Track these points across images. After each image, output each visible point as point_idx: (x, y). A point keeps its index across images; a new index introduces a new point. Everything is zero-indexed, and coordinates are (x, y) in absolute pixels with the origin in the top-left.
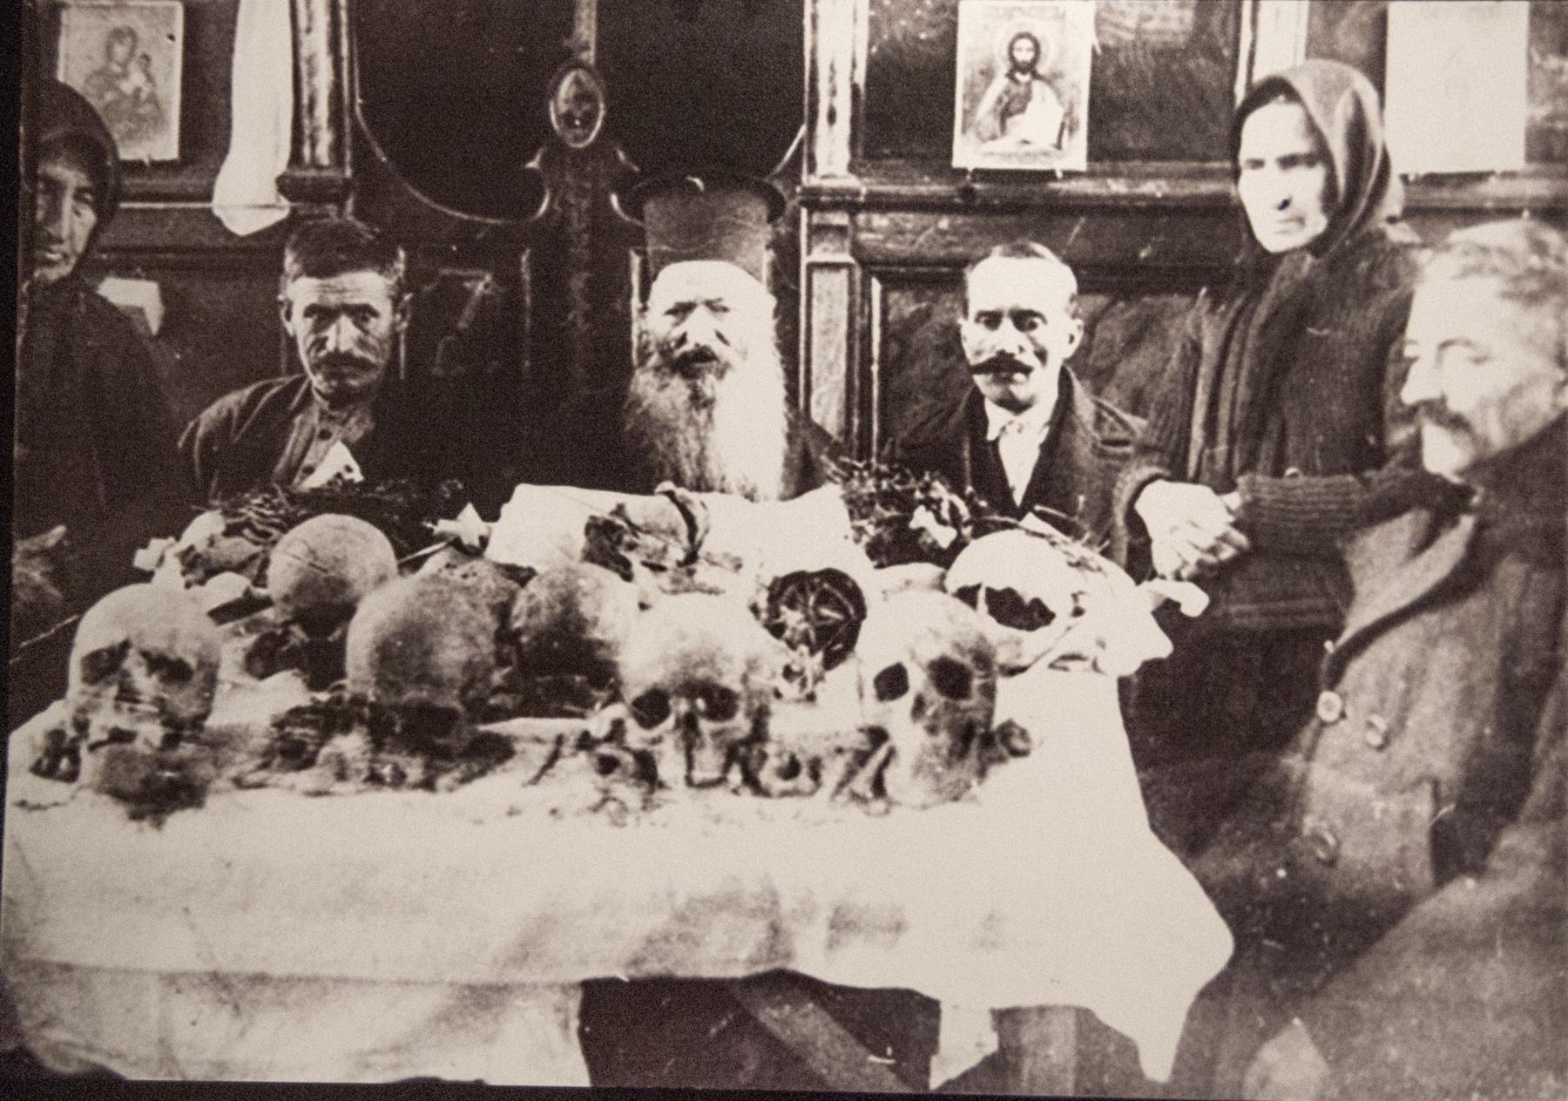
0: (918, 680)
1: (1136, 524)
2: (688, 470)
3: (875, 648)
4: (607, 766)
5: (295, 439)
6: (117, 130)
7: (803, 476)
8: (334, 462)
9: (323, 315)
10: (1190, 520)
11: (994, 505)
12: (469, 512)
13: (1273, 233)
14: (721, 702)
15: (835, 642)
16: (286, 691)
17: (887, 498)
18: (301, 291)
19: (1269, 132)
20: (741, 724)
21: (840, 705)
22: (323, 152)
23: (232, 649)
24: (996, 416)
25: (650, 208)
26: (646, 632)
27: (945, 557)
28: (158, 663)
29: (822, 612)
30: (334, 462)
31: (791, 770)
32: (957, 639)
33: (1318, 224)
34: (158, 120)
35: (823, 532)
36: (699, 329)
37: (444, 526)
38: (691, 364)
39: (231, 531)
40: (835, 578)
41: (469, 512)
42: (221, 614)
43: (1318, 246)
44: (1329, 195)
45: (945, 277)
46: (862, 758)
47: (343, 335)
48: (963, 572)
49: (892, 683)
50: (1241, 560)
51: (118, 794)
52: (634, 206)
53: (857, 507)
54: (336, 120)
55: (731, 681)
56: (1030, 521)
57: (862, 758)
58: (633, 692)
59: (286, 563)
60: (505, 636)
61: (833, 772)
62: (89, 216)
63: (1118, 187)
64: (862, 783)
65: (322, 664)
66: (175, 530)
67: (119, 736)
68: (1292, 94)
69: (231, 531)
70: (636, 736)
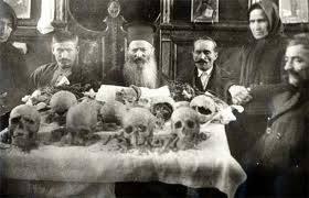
0: (183, 124)
1: (229, 94)
2: (137, 82)
3: (175, 117)
4: (121, 141)
5: (55, 75)
6: (16, 11)
7: (160, 84)
8: (64, 80)
9: (61, 50)
10: (238, 91)
11: (199, 90)
12: (92, 90)
13: (257, 35)
14: (144, 129)
15: (167, 117)
16: (53, 126)
17: (177, 88)
18: (56, 45)
19: (255, 14)
20: (147, 133)
21: (167, 129)
22: (61, 18)
23: (43, 117)
24: (200, 72)
25: (129, 30)
26: (128, 115)
27: (189, 100)
28: (27, 120)
29: (165, 111)
30: (64, 80)
31: (158, 142)
32: (206, 142)
33: (266, 33)
34: (26, 11)
35: (163, 95)
36: (139, 54)
37: (86, 93)
38: (138, 61)
39: (43, 94)
40: (167, 104)
41: (92, 90)
42: (41, 110)
43: (266, 37)
44: (268, 27)
45: (191, 43)
46: (172, 140)
47: (65, 55)
48: (192, 104)
49: (178, 125)
50: (251, 101)
51: (20, 146)
52: (126, 29)
53: (171, 90)
54: (64, 10)
55: (145, 125)
56: (207, 93)
57: (172, 140)
58: (126, 126)
59: (54, 100)
60: (99, 115)
61: (166, 143)
62: (11, 29)
63: (224, 25)
64: (172, 145)
65: (62, 121)
66: (30, 93)
67: (19, 134)
68: (260, 8)
69: (43, 94)
70: (126, 135)
